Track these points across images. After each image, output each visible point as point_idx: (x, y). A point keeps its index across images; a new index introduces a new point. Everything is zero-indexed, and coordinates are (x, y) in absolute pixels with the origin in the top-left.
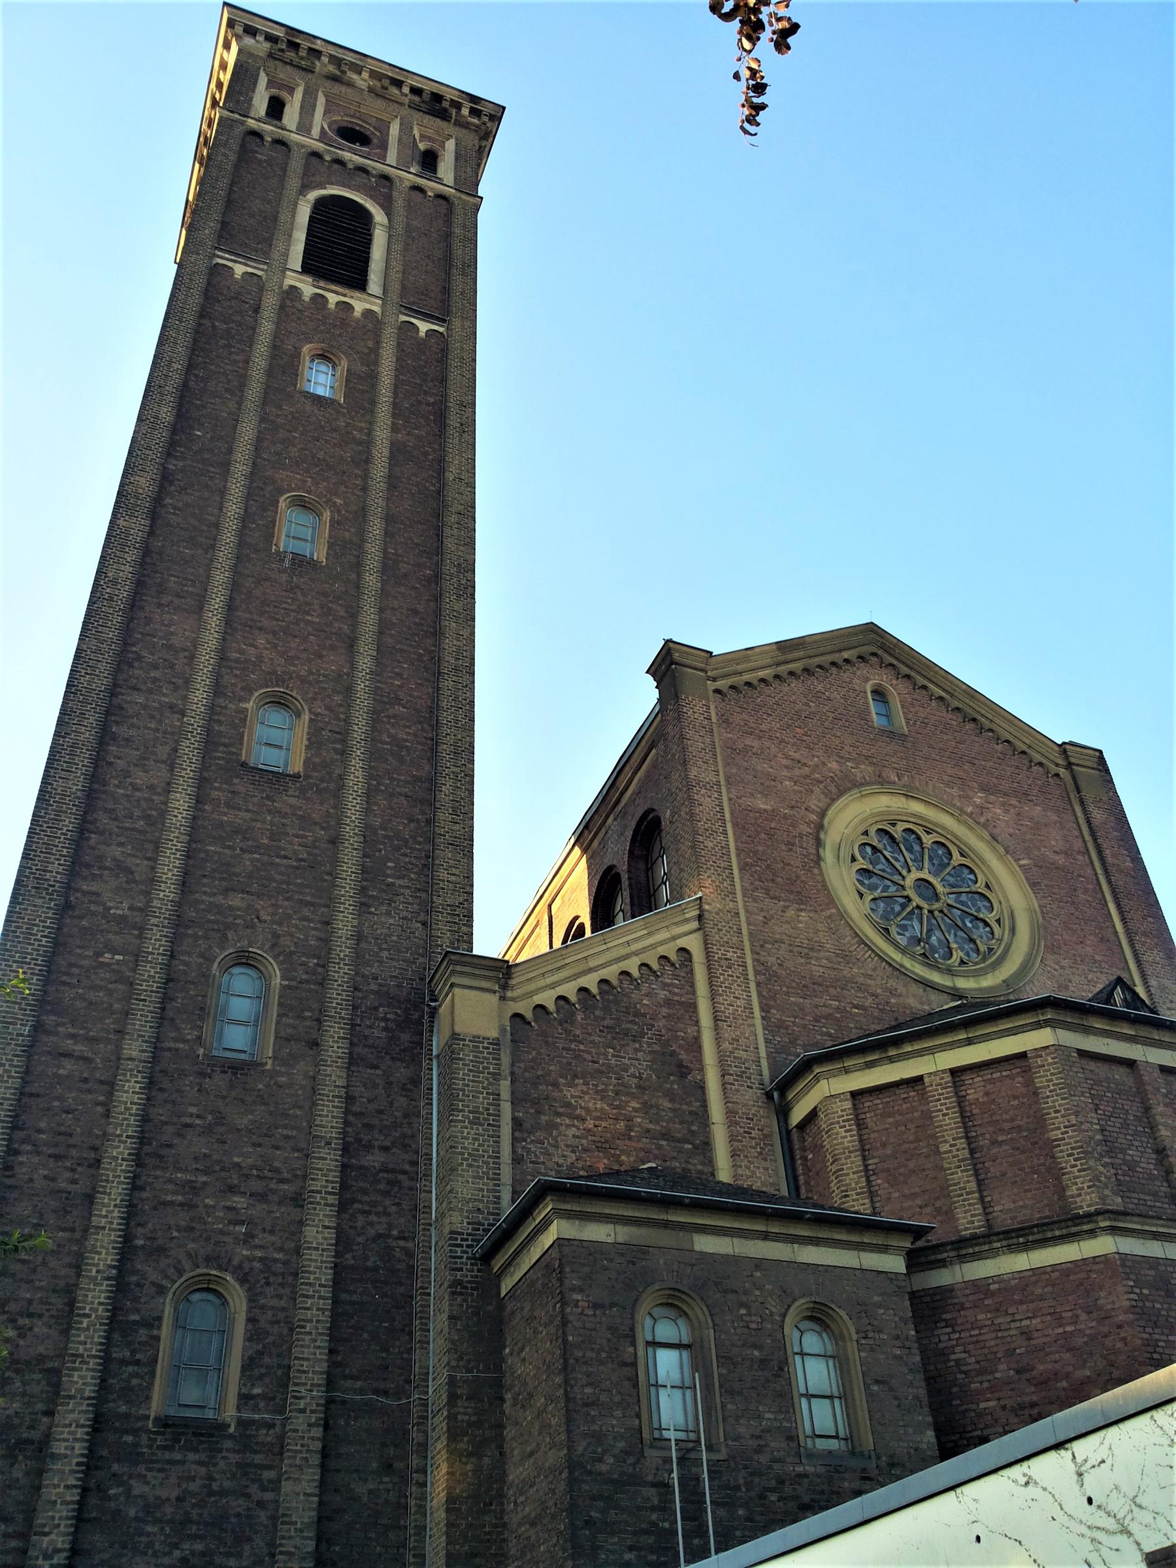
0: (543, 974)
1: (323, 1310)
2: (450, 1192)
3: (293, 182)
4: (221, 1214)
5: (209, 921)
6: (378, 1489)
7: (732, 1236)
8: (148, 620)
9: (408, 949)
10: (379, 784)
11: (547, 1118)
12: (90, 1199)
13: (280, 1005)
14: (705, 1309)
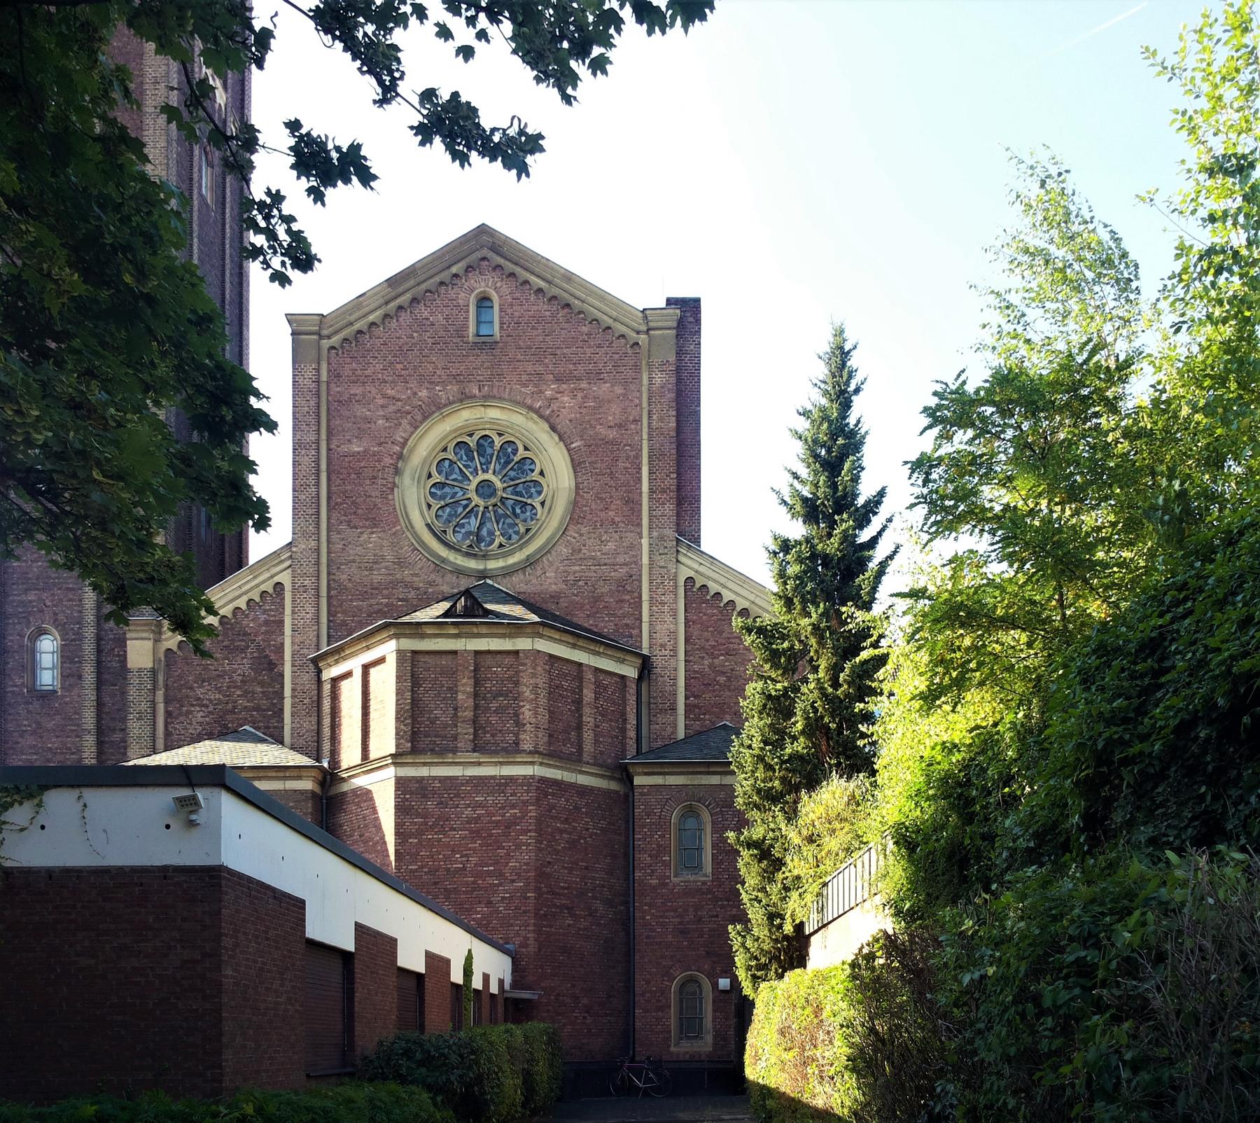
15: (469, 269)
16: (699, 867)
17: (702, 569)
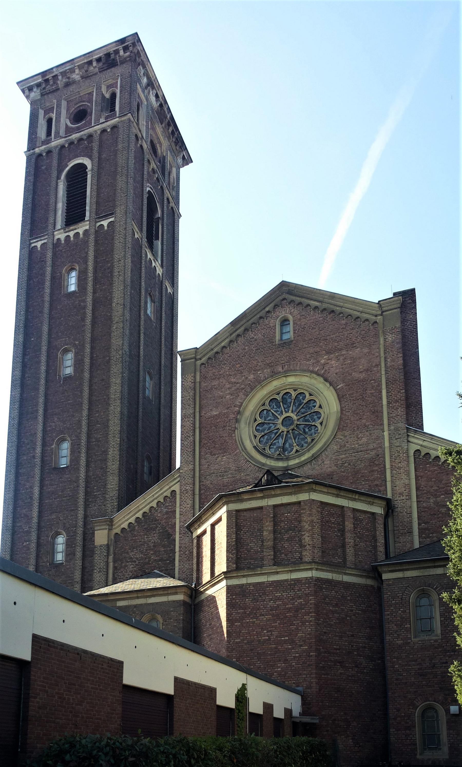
5: (48, 525)
8: (25, 427)
15: (276, 306)
16: (431, 630)
17: (425, 444)
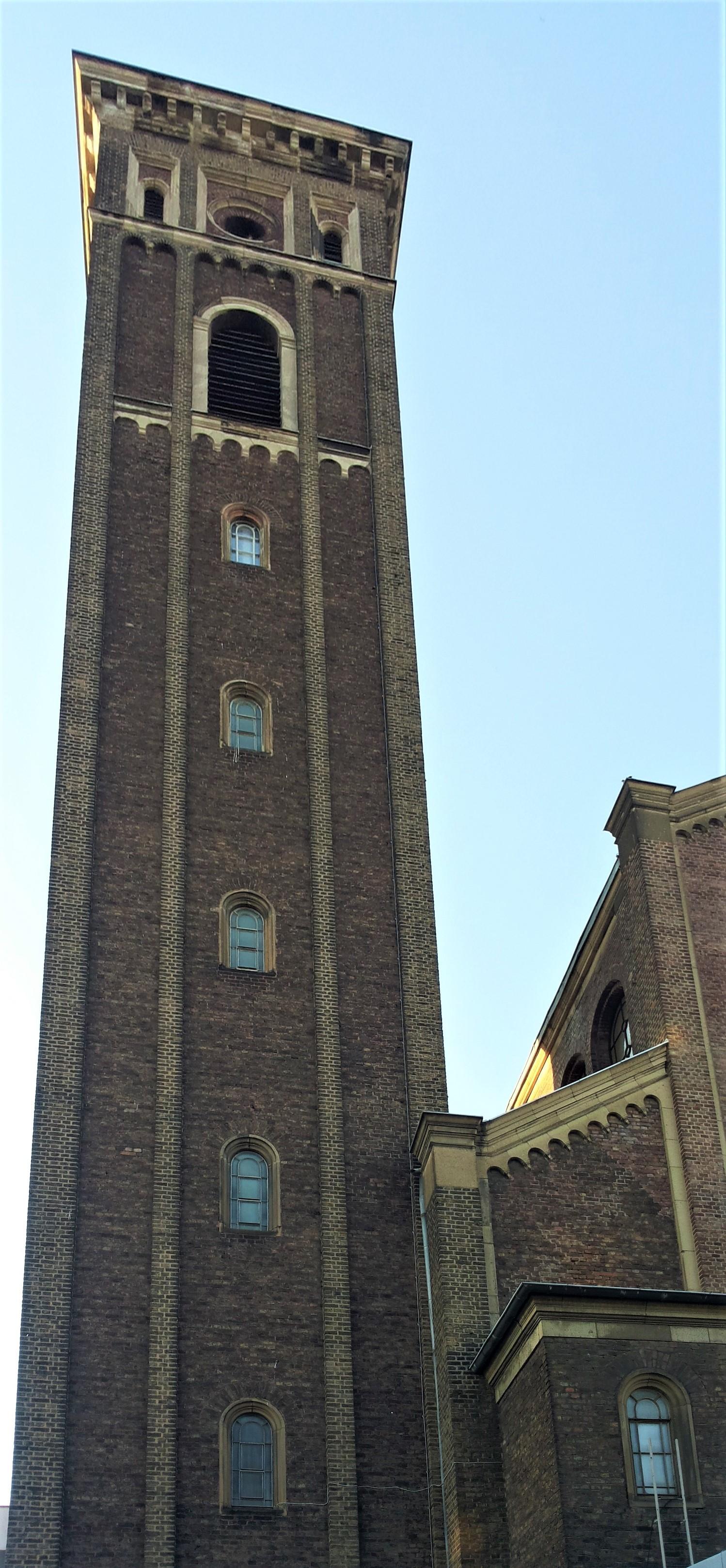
0: (516, 1130)
1: (348, 1424)
2: (445, 1320)
3: (185, 299)
4: (255, 1355)
6: (407, 1553)
7: (708, 1327)
8: (114, 833)
9: (390, 1126)
10: (348, 974)
11: (527, 1256)
12: (145, 1349)
13: (282, 1182)
14: (683, 1388)
